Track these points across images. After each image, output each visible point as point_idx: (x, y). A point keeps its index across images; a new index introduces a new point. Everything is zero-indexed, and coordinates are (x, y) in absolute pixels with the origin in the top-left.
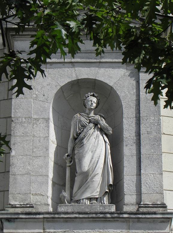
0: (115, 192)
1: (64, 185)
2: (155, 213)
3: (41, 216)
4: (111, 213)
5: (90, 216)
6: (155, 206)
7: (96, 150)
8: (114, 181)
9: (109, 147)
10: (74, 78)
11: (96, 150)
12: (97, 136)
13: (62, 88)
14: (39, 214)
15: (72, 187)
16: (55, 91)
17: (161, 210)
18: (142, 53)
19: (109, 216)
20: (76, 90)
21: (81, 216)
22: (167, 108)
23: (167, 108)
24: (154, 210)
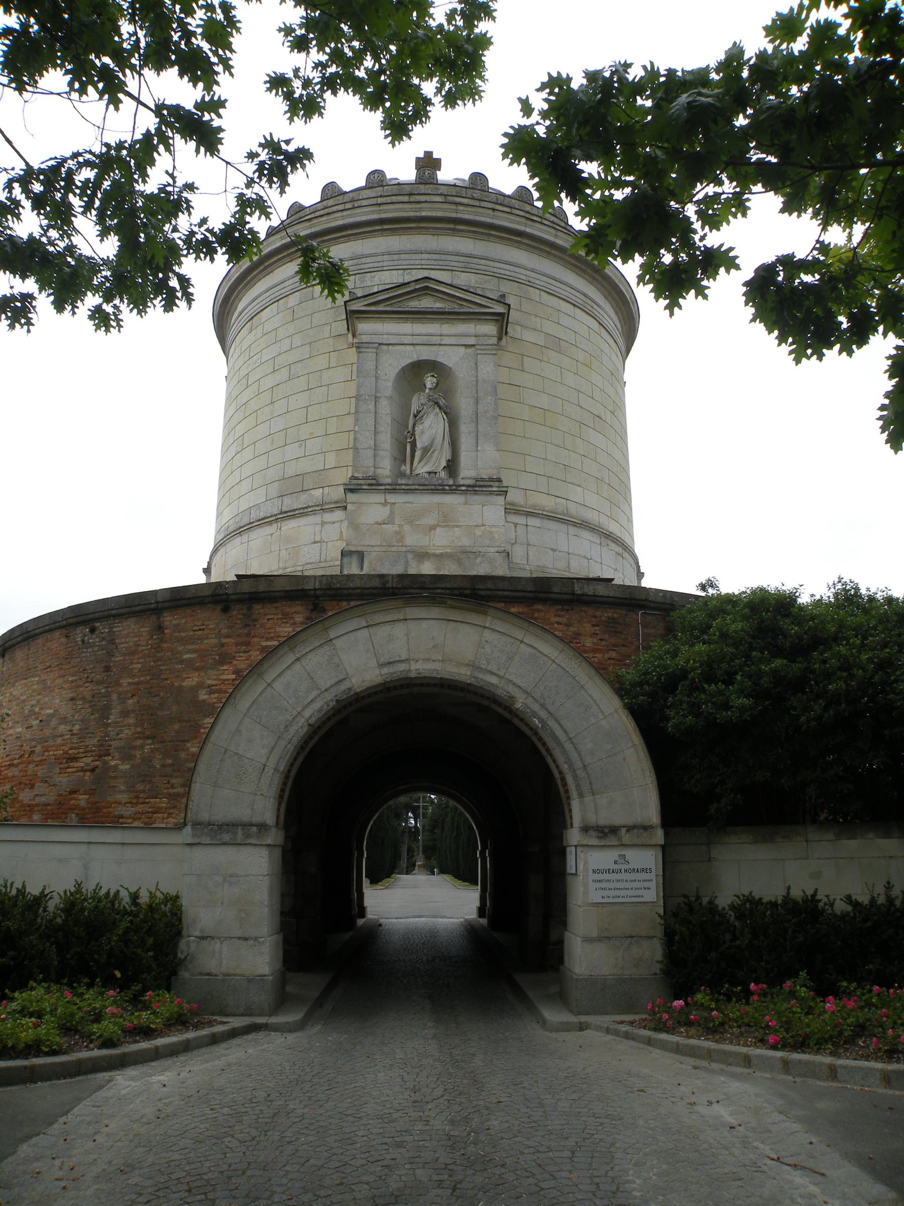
0: (452, 466)
1: (404, 461)
2: (491, 486)
3: (383, 487)
4: (449, 486)
5: (430, 487)
6: (491, 480)
7: (432, 428)
8: (218, 321)
9: (447, 424)
10: (415, 359)
11: (432, 428)
12: (437, 414)
13: (403, 369)
14: (381, 485)
15: (412, 463)
16: (397, 371)
17: (497, 484)
18: (207, 99)
19: (447, 488)
20: (416, 371)
21: (421, 488)
22: (122, 102)
23: (122, 102)
24: (491, 483)
